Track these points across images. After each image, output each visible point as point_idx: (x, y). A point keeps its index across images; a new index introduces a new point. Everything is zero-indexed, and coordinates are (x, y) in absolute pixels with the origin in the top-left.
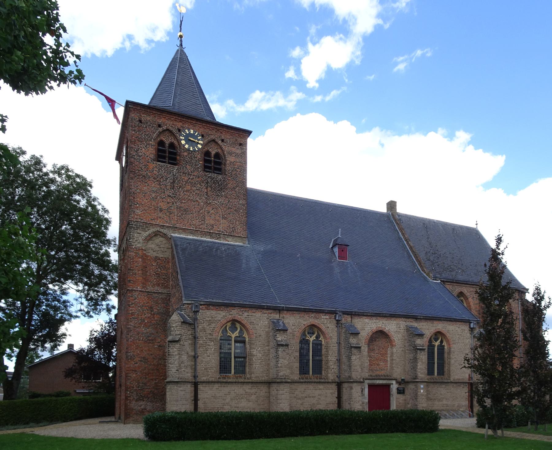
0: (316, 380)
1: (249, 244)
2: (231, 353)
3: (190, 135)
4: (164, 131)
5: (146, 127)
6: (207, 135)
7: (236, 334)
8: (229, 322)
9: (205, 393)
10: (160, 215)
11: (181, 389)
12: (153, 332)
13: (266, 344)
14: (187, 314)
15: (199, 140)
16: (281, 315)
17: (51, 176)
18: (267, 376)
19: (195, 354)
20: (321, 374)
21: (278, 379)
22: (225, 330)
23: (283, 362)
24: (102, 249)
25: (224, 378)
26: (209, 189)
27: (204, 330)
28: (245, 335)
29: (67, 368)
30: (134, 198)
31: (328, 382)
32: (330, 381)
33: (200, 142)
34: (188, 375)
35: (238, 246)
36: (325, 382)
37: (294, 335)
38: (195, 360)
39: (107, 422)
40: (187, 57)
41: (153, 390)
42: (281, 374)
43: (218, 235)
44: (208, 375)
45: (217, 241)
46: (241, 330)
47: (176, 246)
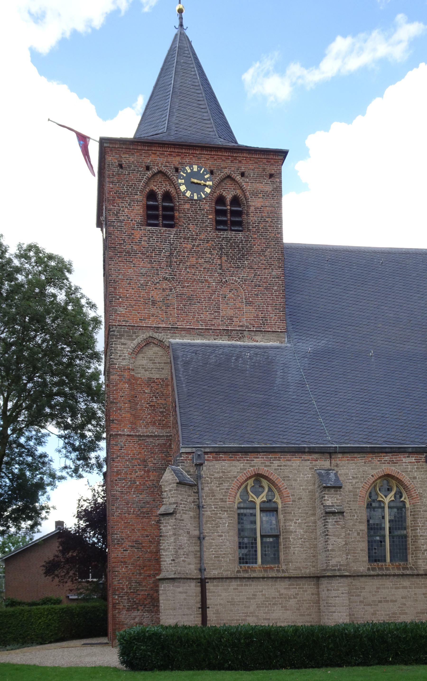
0: (397, 572)
1: (289, 342)
2: (255, 529)
3: (193, 174)
4: (154, 175)
5: (129, 174)
6: (218, 169)
7: (263, 497)
8: (250, 478)
9: (217, 595)
10: (153, 311)
11: (180, 589)
12: (148, 499)
13: (310, 512)
14: (185, 469)
15: (206, 180)
16: (333, 462)
17: (16, 262)
18: (314, 567)
19: (200, 533)
20: (407, 560)
21: (328, 570)
23: (336, 541)
24: (89, 368)
25: (246, 571)
26: (224, 258)
27: (212, 493)
28: (277, 499)
29: (47, 560)
30: (115, 289)
31: (418, 575)
32: (422, 572)
33: (208, 183)
34: (191, 568)
35: (272, 348)
36: (413, 575)
37: (355, 495)
38: (201, 543)
39: (92, 644)
40: (190, 43)
41: (151, 592)
42: (333, 562)
43: (240, 334)
44: (221, 568)
45: (239, 343)
46: (270, 490)
47: (176, 358)
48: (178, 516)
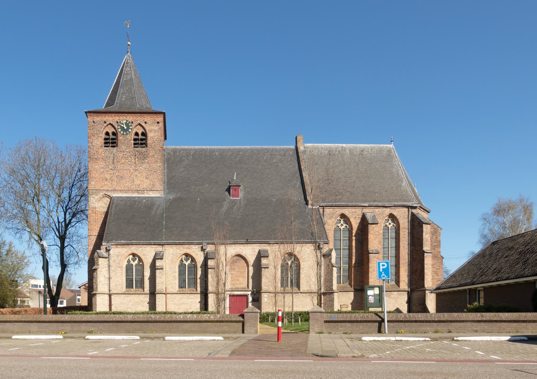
8: (130, 255)
10: (106, 183)
27: (115, 261)
43: (143, 191)
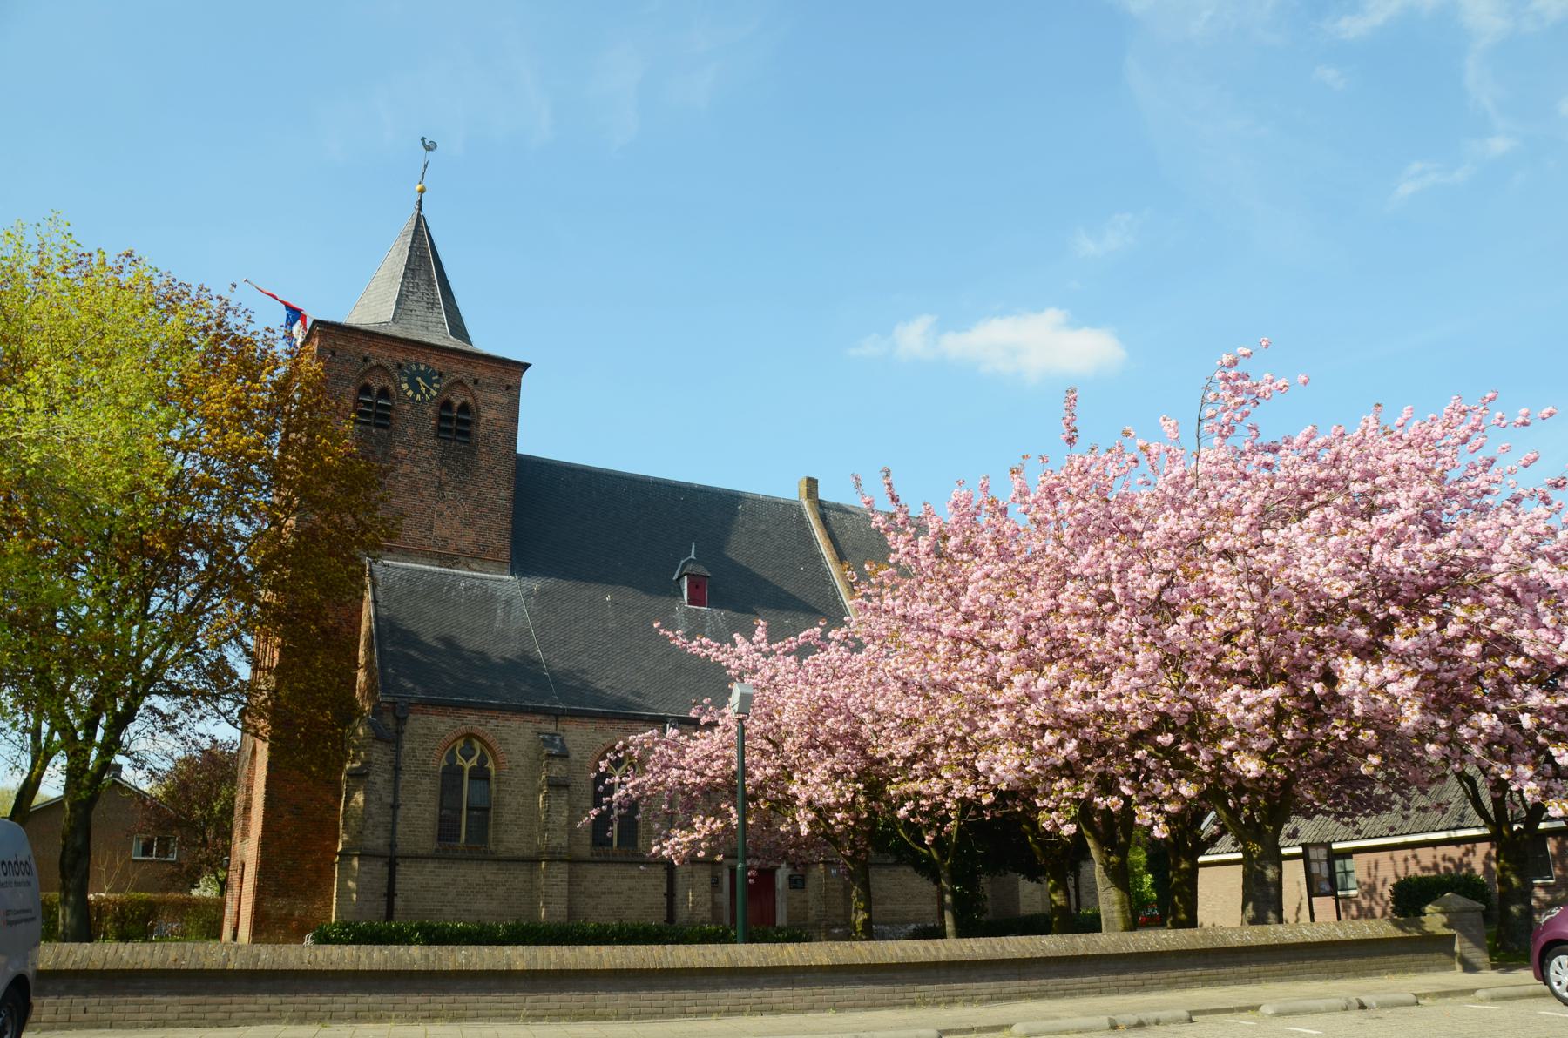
7: (474, 762)
9: (411, 878)
22: (451, 757)
28: (490, 765)
48: (371, 778)
